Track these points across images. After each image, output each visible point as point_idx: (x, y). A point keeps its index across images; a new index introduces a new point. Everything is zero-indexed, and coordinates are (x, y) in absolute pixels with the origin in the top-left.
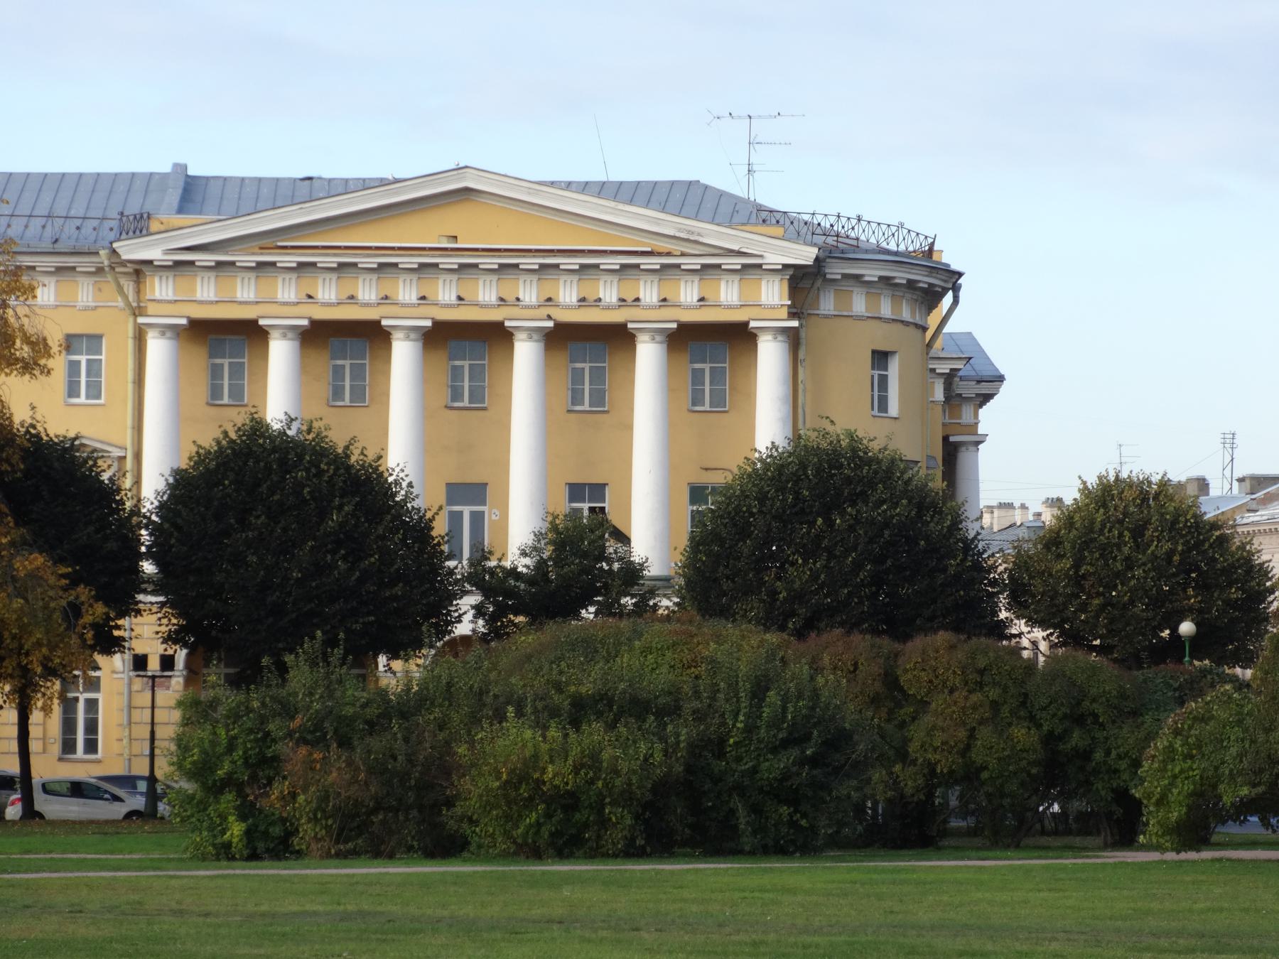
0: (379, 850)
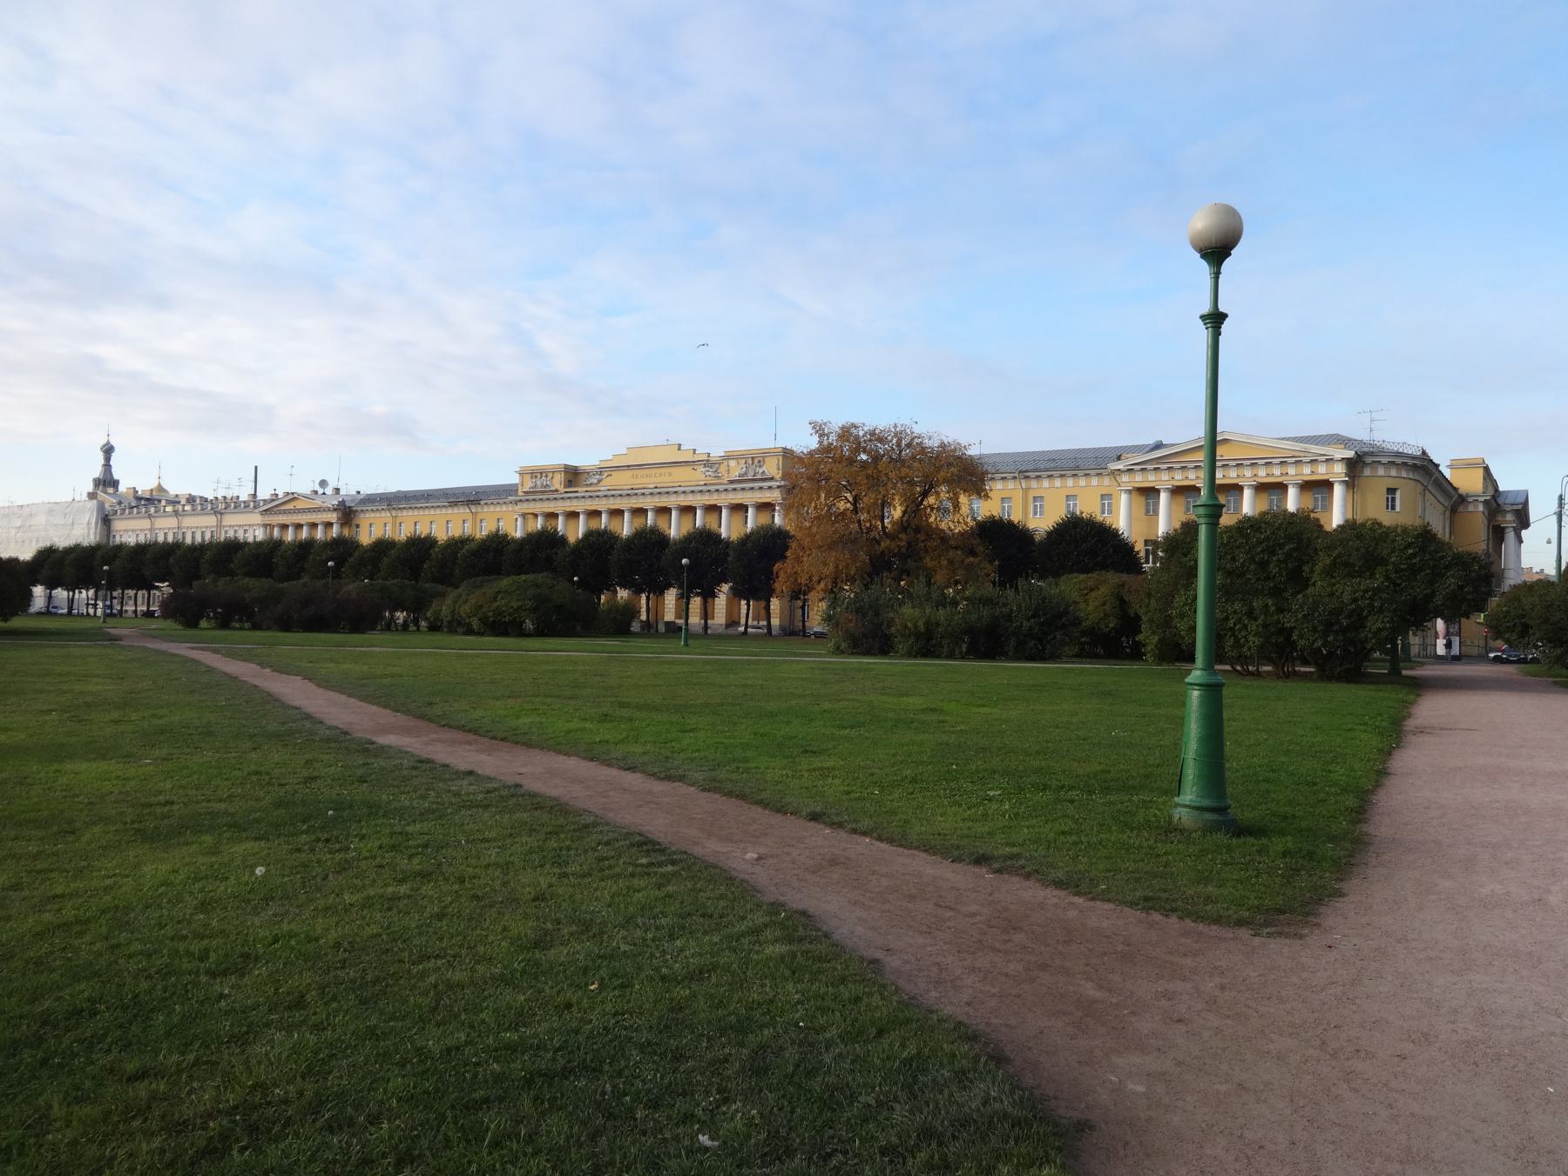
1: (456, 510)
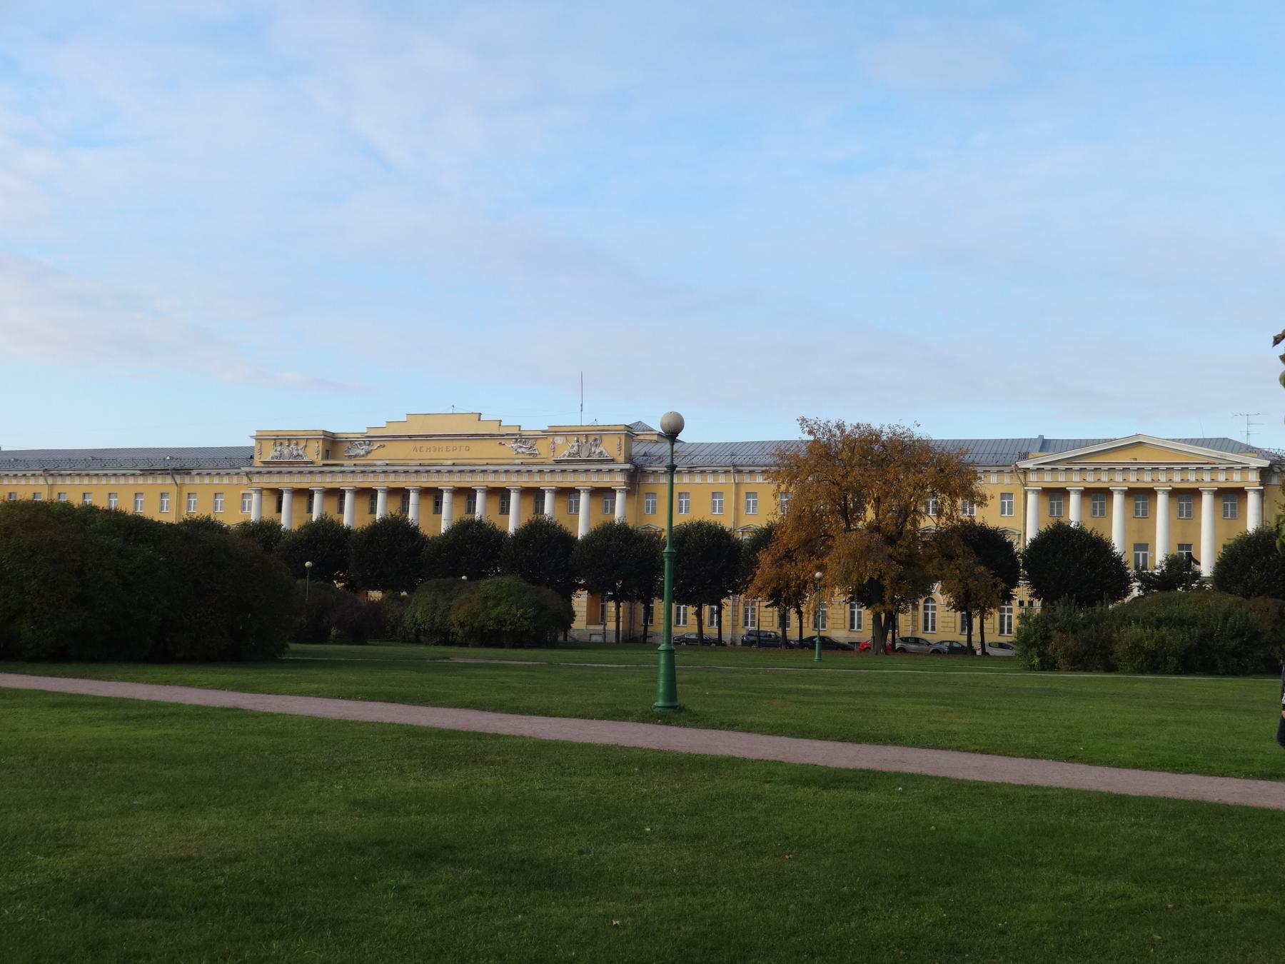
0: (1086, 669)
1: (150, 480)
